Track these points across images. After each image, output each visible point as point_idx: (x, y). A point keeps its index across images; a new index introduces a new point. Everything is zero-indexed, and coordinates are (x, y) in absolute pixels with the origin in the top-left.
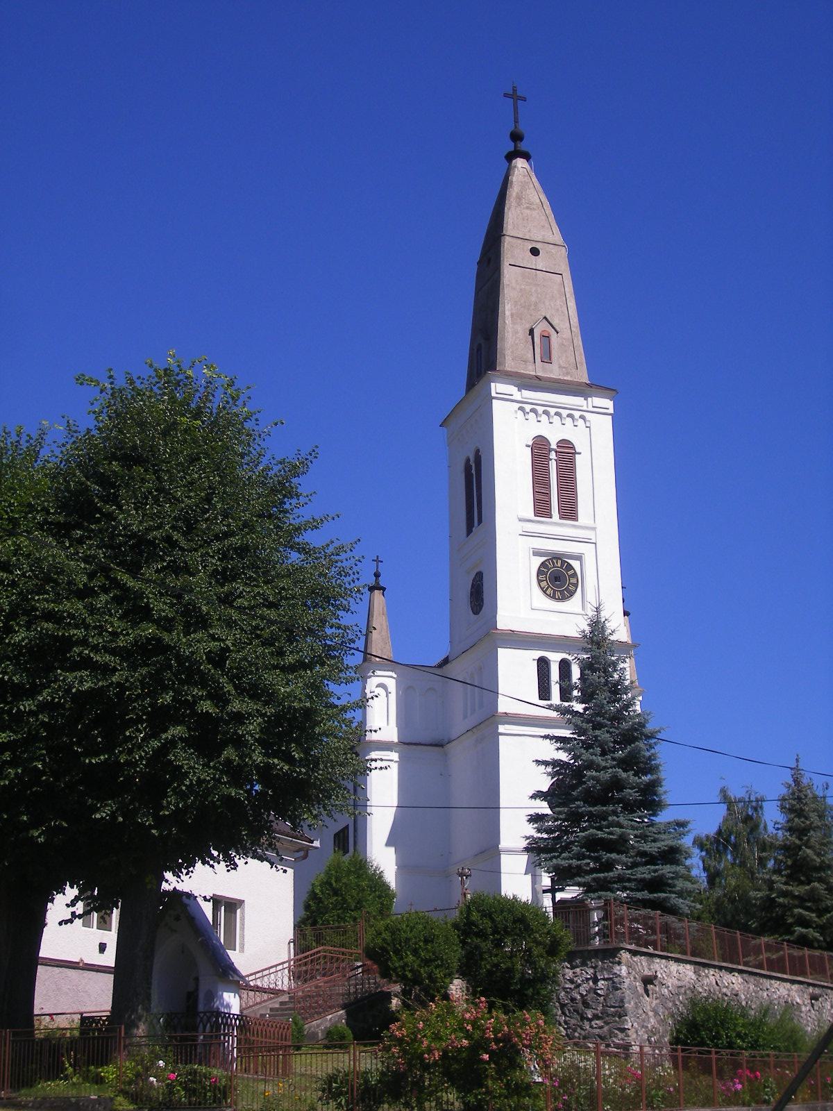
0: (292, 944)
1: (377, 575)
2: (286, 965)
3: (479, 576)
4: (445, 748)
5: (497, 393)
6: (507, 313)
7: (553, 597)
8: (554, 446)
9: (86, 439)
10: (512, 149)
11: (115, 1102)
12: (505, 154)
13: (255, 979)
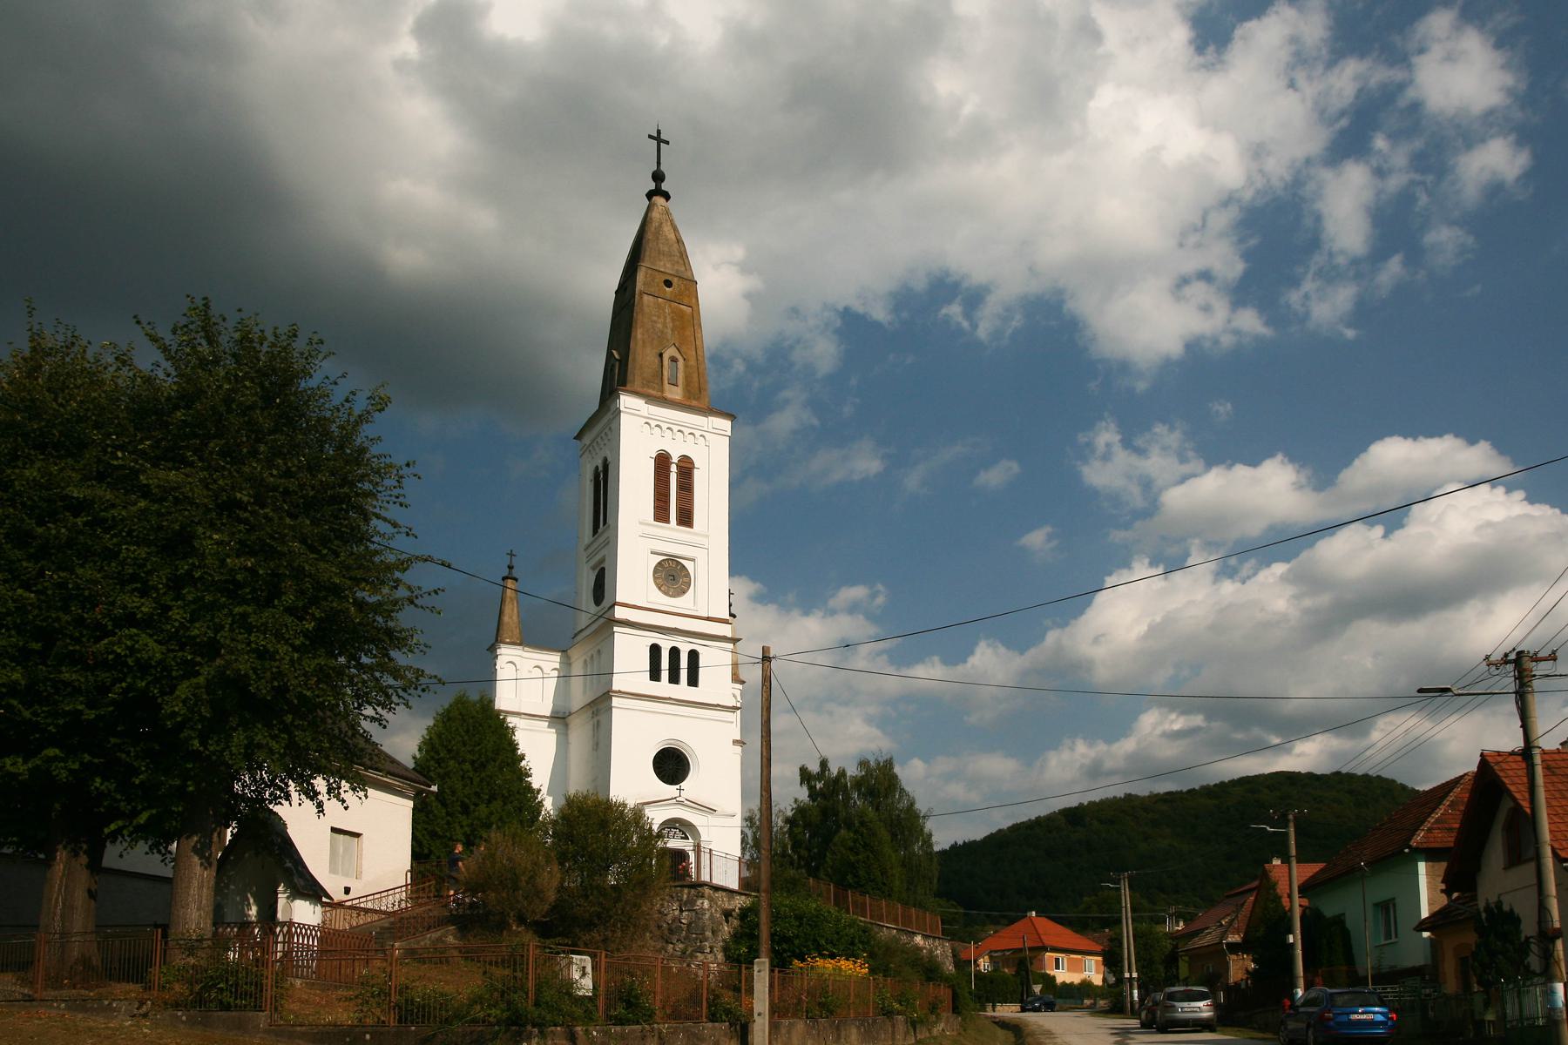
0: (409, 874)
1: (511, 567)
2: (404, 889)
3: (602, 571)
4: (567, 720)
6: (639, 336)
7: (666, 593)
8: (675, 459)
9: (183, 341)
10: (654, 188)
11: (989, 1007)
12: (647, 191)
13: (367, 901)
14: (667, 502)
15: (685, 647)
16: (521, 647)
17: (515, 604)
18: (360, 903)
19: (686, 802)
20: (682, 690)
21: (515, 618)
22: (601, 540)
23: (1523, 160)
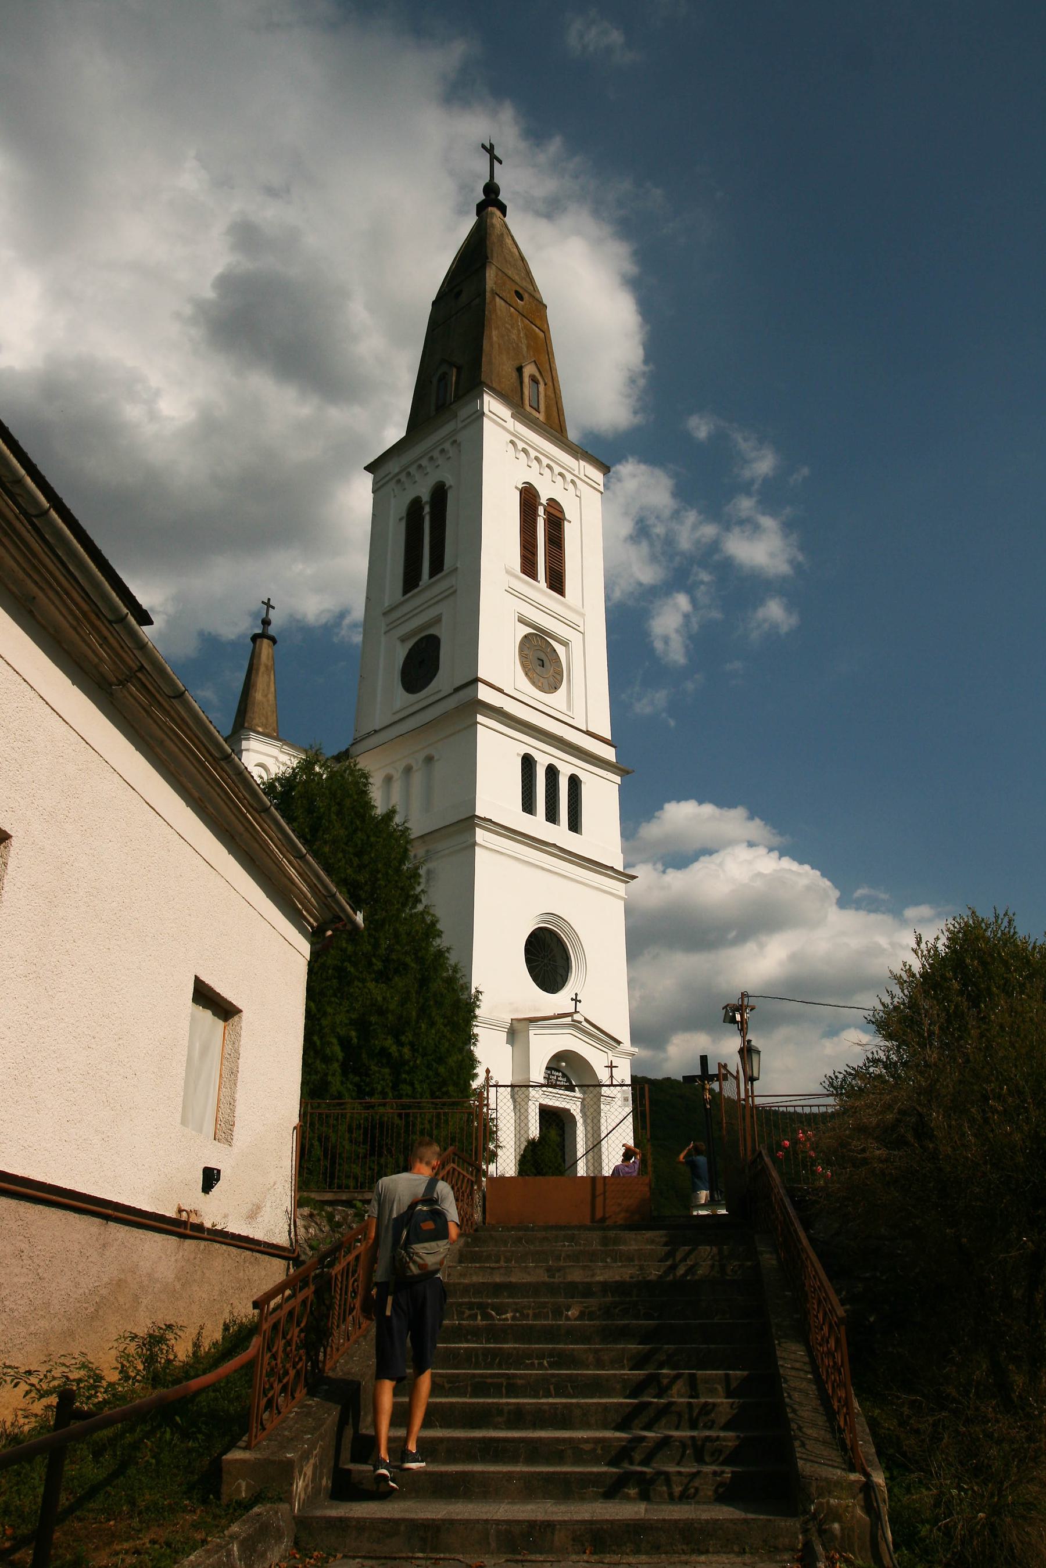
5: (490, 411)
8: (544, 501)
14: (534, 554)
15: (565, 771)
16: (279, 744)
17: (272, 677)
18: (802, 1437)
19: (584, 1023)
20: (559, 834)
21: (271, 697)
22: (443, 585)
23: (794, 620)
